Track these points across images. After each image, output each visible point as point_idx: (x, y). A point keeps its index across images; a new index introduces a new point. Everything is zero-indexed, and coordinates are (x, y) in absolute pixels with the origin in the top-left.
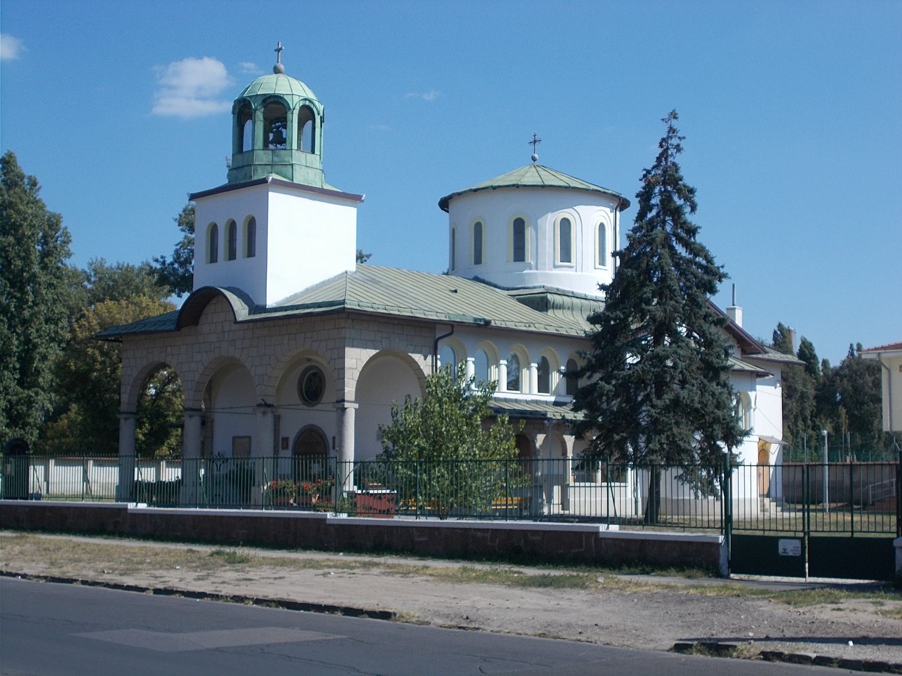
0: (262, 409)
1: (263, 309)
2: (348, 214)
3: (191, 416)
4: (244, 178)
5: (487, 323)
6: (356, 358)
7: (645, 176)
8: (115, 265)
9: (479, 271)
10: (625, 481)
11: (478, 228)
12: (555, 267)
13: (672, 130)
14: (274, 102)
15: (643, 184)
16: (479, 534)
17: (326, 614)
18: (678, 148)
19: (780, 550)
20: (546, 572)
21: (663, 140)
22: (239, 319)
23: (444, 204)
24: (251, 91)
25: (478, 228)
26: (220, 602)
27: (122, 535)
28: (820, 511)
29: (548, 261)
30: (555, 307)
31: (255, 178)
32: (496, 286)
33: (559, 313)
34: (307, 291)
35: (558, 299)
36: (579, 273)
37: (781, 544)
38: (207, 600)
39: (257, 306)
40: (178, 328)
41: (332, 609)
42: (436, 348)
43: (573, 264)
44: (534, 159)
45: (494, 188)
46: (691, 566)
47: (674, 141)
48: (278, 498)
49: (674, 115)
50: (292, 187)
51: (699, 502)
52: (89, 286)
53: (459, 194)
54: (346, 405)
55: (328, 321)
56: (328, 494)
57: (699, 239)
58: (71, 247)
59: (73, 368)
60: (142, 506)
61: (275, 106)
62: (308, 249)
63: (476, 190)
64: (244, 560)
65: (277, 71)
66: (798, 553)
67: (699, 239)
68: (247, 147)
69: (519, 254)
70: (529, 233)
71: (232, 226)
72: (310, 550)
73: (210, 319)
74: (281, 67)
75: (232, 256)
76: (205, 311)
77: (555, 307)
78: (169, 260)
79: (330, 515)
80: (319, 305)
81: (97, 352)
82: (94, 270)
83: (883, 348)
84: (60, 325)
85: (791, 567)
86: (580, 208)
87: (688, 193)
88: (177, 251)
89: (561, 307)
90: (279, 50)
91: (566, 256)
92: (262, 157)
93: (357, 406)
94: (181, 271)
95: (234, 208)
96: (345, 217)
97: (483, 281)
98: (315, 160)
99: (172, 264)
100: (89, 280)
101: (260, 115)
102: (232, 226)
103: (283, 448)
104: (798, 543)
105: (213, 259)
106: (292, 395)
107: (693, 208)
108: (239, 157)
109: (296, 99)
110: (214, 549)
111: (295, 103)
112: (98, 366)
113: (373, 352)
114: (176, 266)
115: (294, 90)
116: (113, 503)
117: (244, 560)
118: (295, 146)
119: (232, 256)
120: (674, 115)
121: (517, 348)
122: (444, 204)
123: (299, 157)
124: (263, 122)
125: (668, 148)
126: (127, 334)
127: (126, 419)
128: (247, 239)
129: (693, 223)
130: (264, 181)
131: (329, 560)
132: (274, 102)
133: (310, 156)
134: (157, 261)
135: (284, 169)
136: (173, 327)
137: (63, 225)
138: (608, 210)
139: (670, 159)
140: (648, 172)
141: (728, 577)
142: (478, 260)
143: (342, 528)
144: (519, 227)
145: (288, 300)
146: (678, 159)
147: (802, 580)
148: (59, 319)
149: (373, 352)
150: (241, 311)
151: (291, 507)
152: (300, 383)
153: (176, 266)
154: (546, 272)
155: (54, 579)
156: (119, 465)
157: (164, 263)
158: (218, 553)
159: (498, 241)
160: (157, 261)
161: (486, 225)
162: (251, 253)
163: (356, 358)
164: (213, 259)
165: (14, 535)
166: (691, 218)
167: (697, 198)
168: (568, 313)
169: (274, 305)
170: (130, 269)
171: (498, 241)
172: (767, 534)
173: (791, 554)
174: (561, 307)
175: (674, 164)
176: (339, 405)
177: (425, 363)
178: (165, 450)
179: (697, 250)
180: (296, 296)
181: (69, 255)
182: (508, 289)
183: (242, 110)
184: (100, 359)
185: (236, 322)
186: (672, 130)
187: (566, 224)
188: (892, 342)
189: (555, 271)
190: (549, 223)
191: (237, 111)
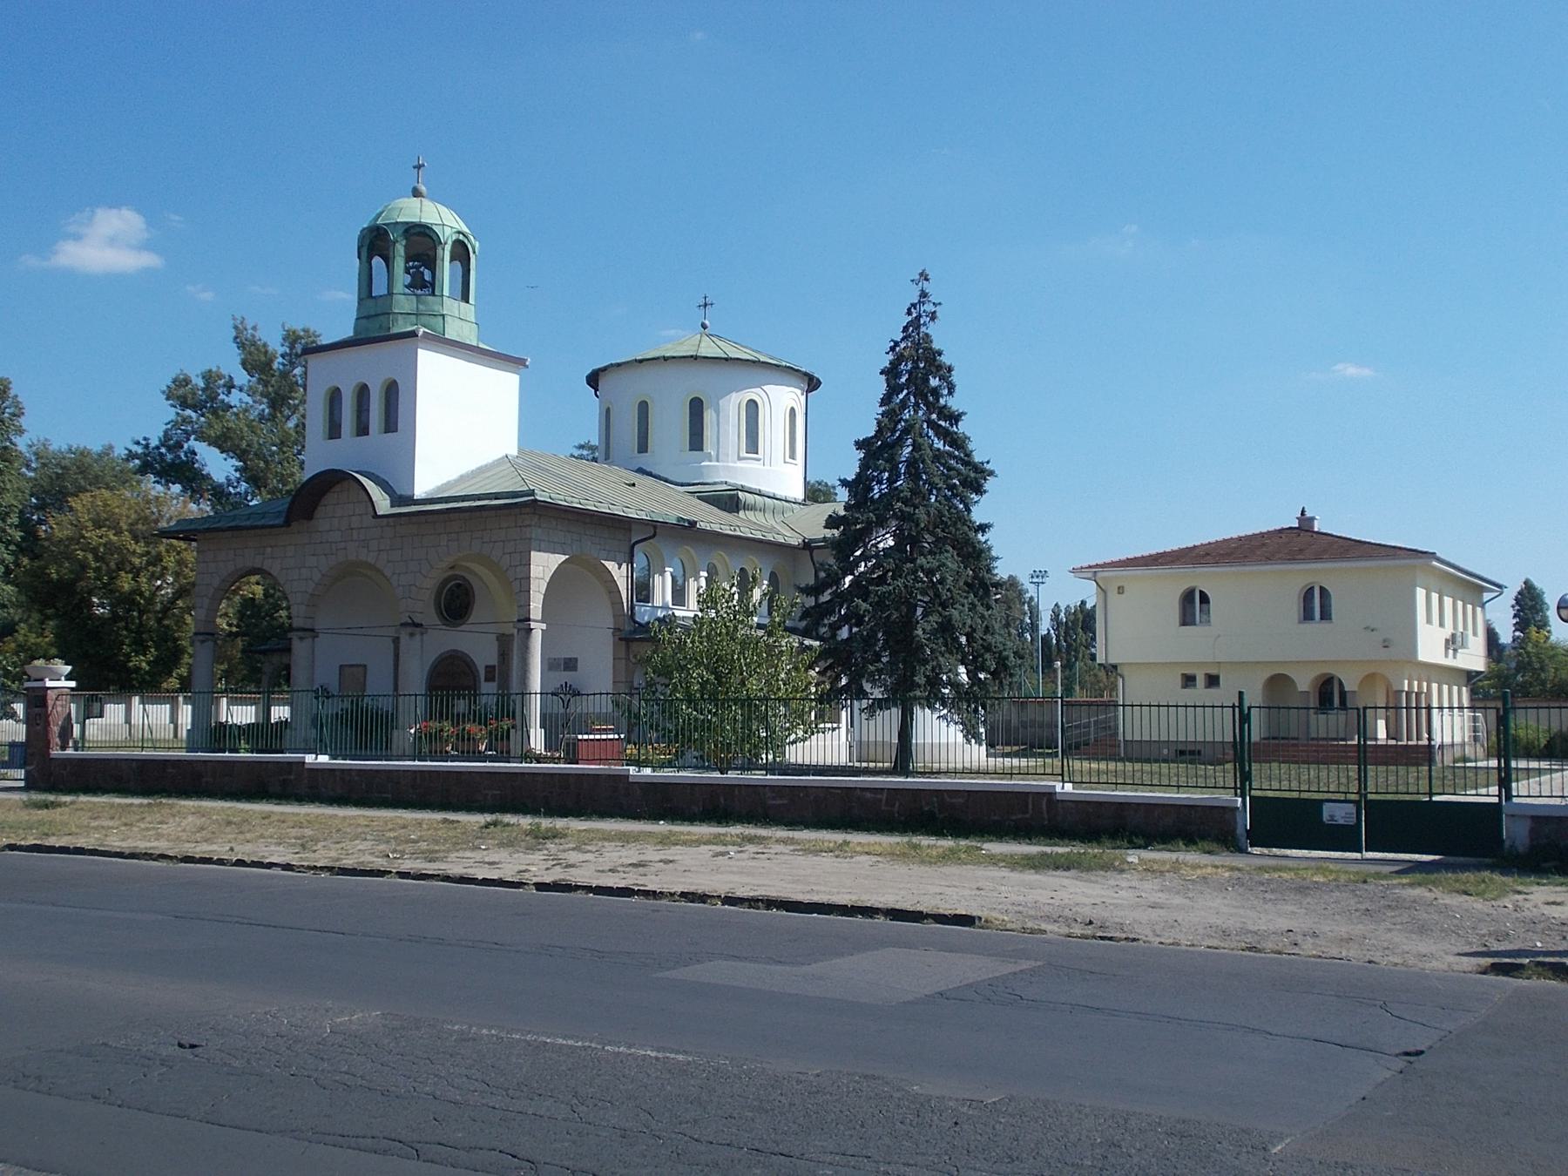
0: (410, 630)
1: (410, 500)
2: (508, 382)
3: (301, 639)
4: (376, 328)
5: (693, 524)
6: (544, 565)
7: (892, 349)
8: (64, 448)
9: (644, 461)
10: (839, 722)
11: (643, 408)
12: (740, 459)
13: (924, 294)
14: (419, 234)
15: (891, 357)
16: (868, 795)
17: (859, 919)
18: (933, 316)
19: (1326, 817)
20: (1048, 849)
21: (914, 305)
22: (380, 513)
23: (593, 380)
24: (387, 218)
25: (643, 408)
26: (664, 902)
27: (300, 799)
28: (1049, 755)
29: (732, 451)
30: (747, 507)
31: (395, 330)
32: (666, 481)
33: (750, 514)
34: (462, 478)
35: (750, 498)
36: (767, 467)
37: (1326, 808)
38: (580, 894)
39: (401, 497)
40: (287, 523)
41: (869, 912)
42: (632, 556)
43: (760, 456)
44: (704, 326)
45: (665, 359)
46: (1204, 837)
47: (929, 308)
48: (429, 745)
49: (924, 276)
50: (442, 342)
51: (1461, 629)
52: (32, 474)
53: (619, 365)
54: (533, 625)
55: (501, 519)
56: (505, 741)
57: (963, 428)
58: (23, 422)
59: (54, 576)
60: (323, 759)
61: (422, 241)
62: (464, 426)
63: (641, 361)
64: (554, 835)
65: (416, 193)
66: (1353, 821)
67: (963, 428)
68: (379, 289)
69: (696, 442)
70: (709, 416)
71: (363, 392)
72: (612, 817)
73: (332, 513)
74: (423, 189)
75: (362, 430)
76: (323, 502)
77: (747, 507)
78: (154, 443)
79: (632, 770)
80: (497, 496)
81: (90, 556)
82: (36, 454)
83: (1097, 566)
84: (9, 521)
85: (1341, 838)
86: (770, 388)
87: (945, 372)
88: (166, 432)
89: (753, 508)
90: (419, 167)
91: (753, 446)
92: (404, 302)
93: (544, 626)
94: (169, 457)
95: (370, 366)
96: (504, 385)
97: (650, 474)
98: (468, 310)
99: (157, 448)
100: (28, 467)
101: (400, 249)
102: (363, 392)
103: (487, 680)
104: (1351, 808)
105: (334, 431)
106: (430, 616)
107: (951, 389)
108: (370, 303)
109: (448, 231)
110: (489, 818)
111: (447, 236)
112: (92, 574)
113: (564, 558)
114: (163, 450)
115: (446, 221)
116: (183, 754)
117: (554, 835)
118: (446, 293)
119: (362, 430)
120: (924, 276)
121: (718, 557)
122: (593, 380)
123: (451, 306)
124: (403, 256)
125: (919, 316)
126: (208, 530)
127: (301, 639)
128: (390, 408)
129: (954, 408)
130: (413, 334)
131: (689, 833)
132: (419, 234)
133: (463, 304)
134: (138, 443)
135: (433, 321)
136: (280, 521)
137: (12, 393)
138: (799, 392)
139: (923, 329)
140: (896, 344)
141: (1243, 851)
142: (643, 447)
143: (650, 787)
144: (696, 408)
145: (439, 489)
146: (932, 329)
147: (1357, 855)
148: (7, 514)
149: (564, 558)
150: (383, 504)
151: (484, 759)
152: (439, 594)
153: (163, 450)
154: (728, 466)
155: (344, 871)
156: (291, 704)
157: (147, 446)
158: (495, 824)
159: (669, 426)
160: (138, 443)
161: (643, 403)
162: (390, 425)
163: (544, 565)
164: (334, 431)
165: (145, 801)
166: (954, 403)
167: (955, 377)
168: (760, 515)
169: (424, 496)
170: (84, 453)
171: (669, 426)
172: (1305, 795)
173: (1341, 822)
174: (753, 508)
175: (927, 335)
176: (521, 625)
177: (619, 574)
178: (173, 683)
179: (957, 442)
180: (448, 485)
181: (20, 431)
182: (682, 485)
183: (375, 242)
184: (93, 565)
185: (376, 516)
186: (924, 294)
187: (752, 406)
188: (1123, 558)
189: (740, 464)
190: (733, 404)
191: (367, 242)
